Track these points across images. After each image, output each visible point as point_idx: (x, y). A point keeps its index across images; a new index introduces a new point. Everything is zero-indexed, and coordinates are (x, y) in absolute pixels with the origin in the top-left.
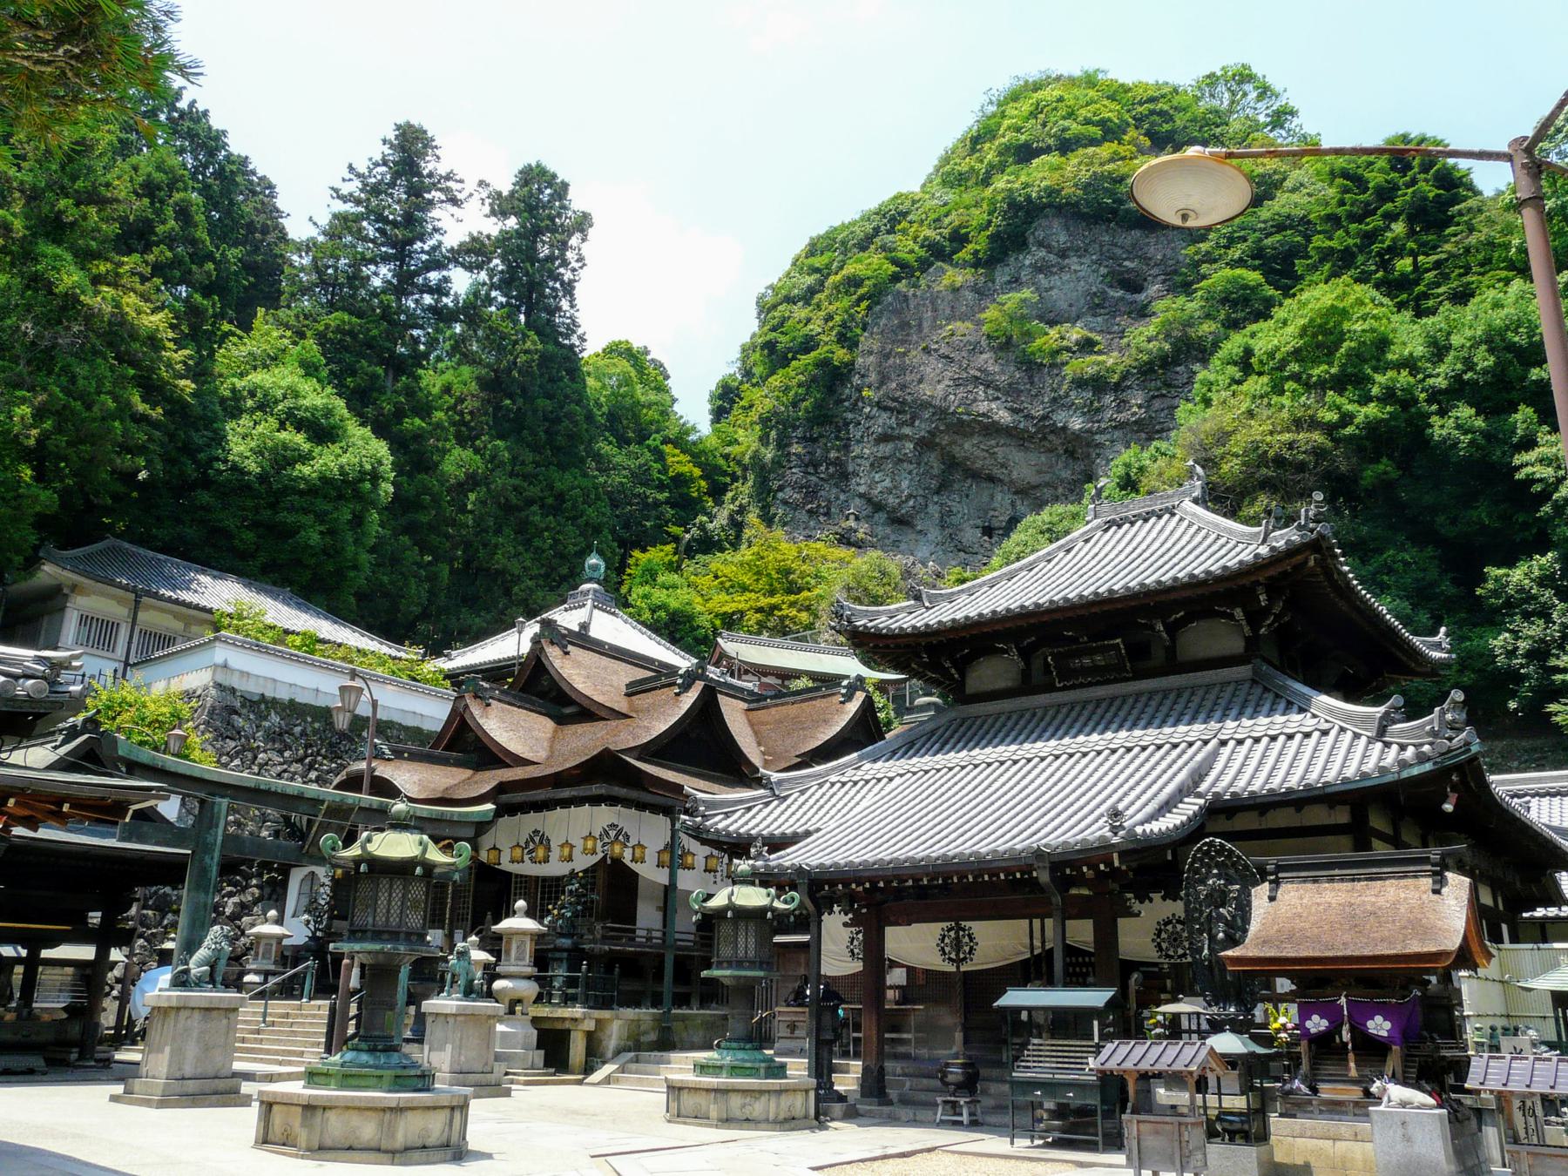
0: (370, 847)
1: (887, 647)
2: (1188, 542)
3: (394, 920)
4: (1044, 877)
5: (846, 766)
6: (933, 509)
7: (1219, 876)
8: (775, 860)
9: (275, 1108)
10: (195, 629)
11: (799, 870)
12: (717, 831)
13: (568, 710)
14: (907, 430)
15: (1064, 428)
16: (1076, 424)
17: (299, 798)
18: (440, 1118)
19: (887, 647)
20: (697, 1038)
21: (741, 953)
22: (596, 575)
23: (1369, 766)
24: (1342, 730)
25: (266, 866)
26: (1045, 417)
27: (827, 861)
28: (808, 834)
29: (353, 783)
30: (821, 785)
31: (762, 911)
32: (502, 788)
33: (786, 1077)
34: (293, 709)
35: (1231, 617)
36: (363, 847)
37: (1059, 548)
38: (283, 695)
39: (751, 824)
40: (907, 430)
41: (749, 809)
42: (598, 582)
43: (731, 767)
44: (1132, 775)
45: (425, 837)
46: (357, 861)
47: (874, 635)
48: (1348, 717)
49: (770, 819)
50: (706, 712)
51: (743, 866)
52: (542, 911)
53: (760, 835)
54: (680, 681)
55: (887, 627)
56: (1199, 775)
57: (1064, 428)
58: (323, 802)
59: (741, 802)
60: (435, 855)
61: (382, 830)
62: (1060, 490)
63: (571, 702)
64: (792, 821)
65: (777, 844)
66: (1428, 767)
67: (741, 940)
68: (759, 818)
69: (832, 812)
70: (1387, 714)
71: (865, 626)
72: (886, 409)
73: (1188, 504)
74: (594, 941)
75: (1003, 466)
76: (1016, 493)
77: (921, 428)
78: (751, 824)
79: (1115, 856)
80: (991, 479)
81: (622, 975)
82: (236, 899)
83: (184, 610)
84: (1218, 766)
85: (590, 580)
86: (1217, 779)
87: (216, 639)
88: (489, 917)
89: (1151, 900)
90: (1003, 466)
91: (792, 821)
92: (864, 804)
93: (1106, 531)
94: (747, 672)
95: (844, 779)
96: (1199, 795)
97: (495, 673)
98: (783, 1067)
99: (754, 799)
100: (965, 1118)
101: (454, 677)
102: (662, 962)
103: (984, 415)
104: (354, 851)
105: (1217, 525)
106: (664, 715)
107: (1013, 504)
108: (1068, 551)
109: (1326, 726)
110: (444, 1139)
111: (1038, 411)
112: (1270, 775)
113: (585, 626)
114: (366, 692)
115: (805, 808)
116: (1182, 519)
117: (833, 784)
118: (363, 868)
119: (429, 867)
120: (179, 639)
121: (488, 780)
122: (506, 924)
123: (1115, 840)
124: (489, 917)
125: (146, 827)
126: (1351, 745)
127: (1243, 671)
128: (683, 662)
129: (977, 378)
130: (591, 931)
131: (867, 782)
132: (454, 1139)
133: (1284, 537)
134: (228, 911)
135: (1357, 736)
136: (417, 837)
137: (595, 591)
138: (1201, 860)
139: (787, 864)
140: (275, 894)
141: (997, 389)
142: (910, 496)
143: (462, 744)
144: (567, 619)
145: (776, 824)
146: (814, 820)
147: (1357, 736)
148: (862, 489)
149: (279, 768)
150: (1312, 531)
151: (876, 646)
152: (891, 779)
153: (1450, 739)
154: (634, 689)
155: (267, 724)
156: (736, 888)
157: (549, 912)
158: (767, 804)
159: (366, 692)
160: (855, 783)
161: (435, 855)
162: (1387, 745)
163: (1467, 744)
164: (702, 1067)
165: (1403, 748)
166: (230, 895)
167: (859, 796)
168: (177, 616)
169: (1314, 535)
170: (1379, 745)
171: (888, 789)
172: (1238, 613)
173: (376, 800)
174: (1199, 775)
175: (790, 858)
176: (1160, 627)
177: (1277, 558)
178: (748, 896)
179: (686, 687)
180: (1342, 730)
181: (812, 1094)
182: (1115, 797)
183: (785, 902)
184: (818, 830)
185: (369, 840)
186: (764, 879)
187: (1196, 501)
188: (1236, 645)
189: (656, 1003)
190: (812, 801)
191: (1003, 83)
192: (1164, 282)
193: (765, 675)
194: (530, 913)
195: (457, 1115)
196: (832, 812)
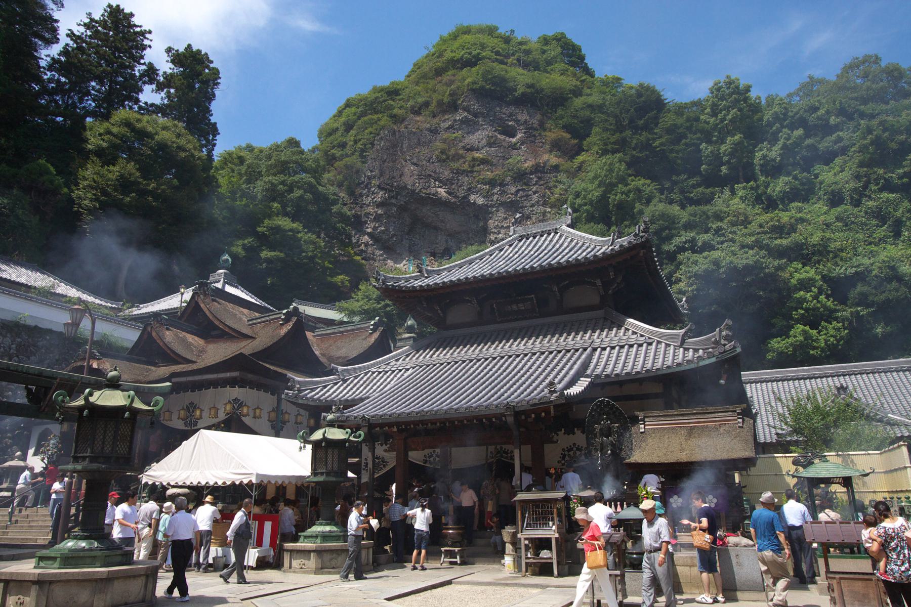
0: (91, 399)
2: (574, 242)
4: (510, 420)
5: (380, 362)
6: (406, 243)
7: (607, 419)
8: (347, 413)
9: (11, 584)
12: (307, 399)
14: (394, 201)
15: (474, 203)
16: (481, 201)
18: (140, 582)
20: (450, 543)
21: (330, 467)
23: (679, 359)
24: (658, 342)
26: (465, 197)
29: (80, 369)
30: (366, 374)
31: (343, 441)
35: (594, 285)
36: (86, 399)
37: (496, 249)
40: (394, 201)
41: (325, 387)
44: (547, 366)
46: (80, 409)
48: (663, 335)
54: (283, 317)
56: (585, 365)
57: (474, 203)
58: (56, 379)
60: (139, 405)
62: (471, 235)
64: (350, 393)
65: (349, 404)
66: (714, 360)
68: (331, 391)
69: (375, 387)
70: (686, 333)
72: (383, 189)
73: (564, 227)
75: (442, 221)
76: (449, 235)
77: (402, 200)
79: (552, 407)
80: (436, 228)
84: (594, 361)
86: (595, 368)
89: (574, 433)
90: (442, 221)
91: (350, 393)
93: (520, 241)
96: (587, 376)
99: (328, 381)
100: (458, 560)
103: (434, 195)
104: (80, 402)
105: (583, 237)
107: (447, 241)
108: (501, 250)
109: (651, 341)
110: (141, 597)
111: (461, 194)
112: (624, 366)
115: (358, 386)
116: (561, 236)
117: (373, 373)
119: (135, 412)
121: (164, 370)
123: (552, 398)
126: (665, 350)
127: (600, 313)
129: (430, 176)
131: (394, 371)
132: (148, 597)
133: (624, 241)
135: (667, 345)
138: (595, 410)
141: (440, 181)
142: (394, 235)
147: (667, 345)
148: (369, 230)
150: (642, 237)
152: (407, 370)
153: (725, 345)
154: (252, 324)
160: (387, 372)
162: (686, 349)
163: (734, 347)
165: (696, 350)
169: (644, 239)
170: (681, 349)
171: (406, 375)
172: (598, 282)
174: (585, 365)
175: (358, 411)
176: (556, 289)
177: (623, 250)
178: (334, 433)
180: (658, 342)
181: (371, 550)
182: (552, 376)
184: (368, 398)
185: (91, 394)
187: (568, 226)
188: (596, 300)
190: (361, 382)
191: (447, 30)
192: (525, 133)
195: (151, 580)
196: (375, 387)
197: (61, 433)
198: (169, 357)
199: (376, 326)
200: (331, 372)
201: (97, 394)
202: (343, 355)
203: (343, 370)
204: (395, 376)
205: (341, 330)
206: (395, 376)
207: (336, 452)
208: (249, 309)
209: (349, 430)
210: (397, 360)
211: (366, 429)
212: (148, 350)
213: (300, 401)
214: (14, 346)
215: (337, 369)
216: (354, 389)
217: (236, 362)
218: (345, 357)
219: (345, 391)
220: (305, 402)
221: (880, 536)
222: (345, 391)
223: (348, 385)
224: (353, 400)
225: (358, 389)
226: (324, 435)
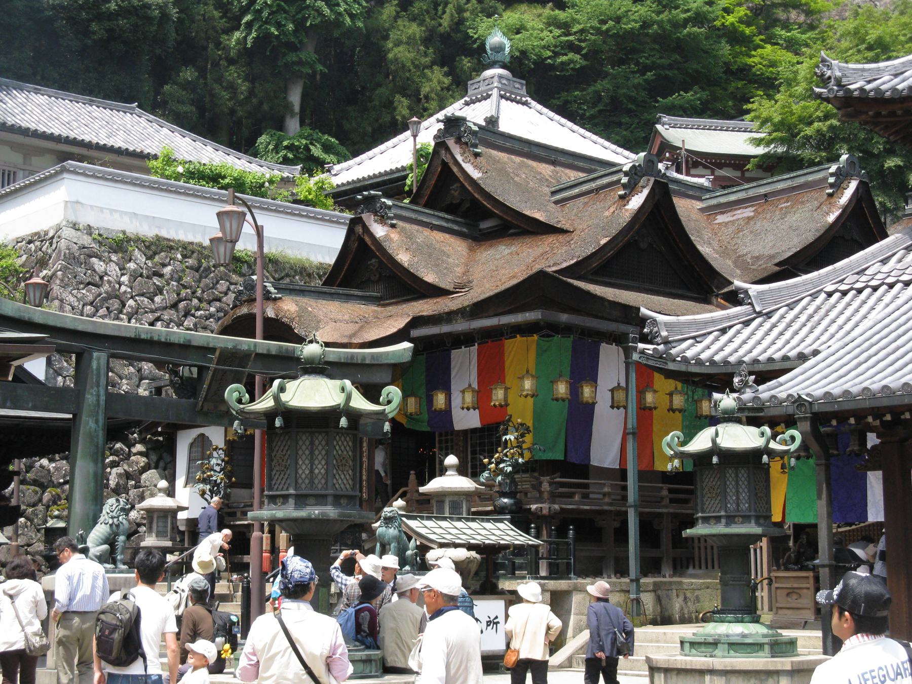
0: (284, 397)
1: (893, 114)
3: (319, 482)
8: (765, 391)
10: (35, 161)
11: (799, 401)
12: (685, 360)
13: (485, 225)
17: (186, 348)
19: (893, 114)
22: (499, 57)
25: (151, 428)
27: (836, 389)
28: (802, 358)
32: (417, 321)
33: (798, 655)
34: (156, 247)
36: (276, 398)
38: (148, 231)
39: (728, 350)
41: (724, 331)
42: (504, 66)
43: (700, 282)
45: (348, 383)
46: (270, 415)
47: (875, 100)
49: (751, 342)
50: (660, 214)
51: (727, 401)
52: (474, 467)
53: (740, 362)
54: (625, 180)
55: (894, 89)
58: (213, 350)
59: (713, 322)
60: (359, 402)
61: (294, 378)
63: (488, 215)
64: (780, 343)
65: (766, 373)
67: (731, 490)
69: (832, 329)
71: (861, 89)
74: (539, 500)
78: (728, 350)
81: (577, 539)
82: (119, 470)
83: (20, 139)
85: (491, 65)
87: (64, 170)
88: (412, 476)
91: (780, 343)
92: (874, 316)
94: (696, 165)
95: (844, 287)
97: (391, 184)
98: (792, 643)
101: (347, 197)
102: (625, 523)
104: (265, 403)
106: (598, 222)
113: (492, 121)
114: (249, 217)
115: (796, 326)
117: (830, 295)
118: (278, 423)
119: (355, 416)
120: (20, 174)
121: (396, 318)
122: (436, 484)
124: (412, 476)
125: (20, 389)
128: (625, 159)
130: (537, 487)
134: (112, 483)
136: (338, 383)
137: (501, 77)
139: (783, 395)
140: (163, 458)
143: (362, 271)
144: (475, 114)
145: (760, 348)
146: (809, 340)
149: (151, 317)
151: (878, 114)
154: (562, 196)
155: (132, 265)
156: (721, 427)
157: (484, 468)
158: (747, 323)
159: (249, 217)
161: (359, 402)
164: (693, 644)
166: (114, 465)
167: (866, 308)
168: (14, 146)
173: (274, 345)
175: (784, 388)
179: (632, 188)
183: (784, 442)
184: (816, 353)
185: (282, 389)
186: (752, 416)
189: (622, 571)
190: (803, 318)
193: (720, 166)
194: (462, 470)
196: (832, 329)
197: (227, 442)
198: (402, 285)
199: (842, 177)
200: (735, 298)
201: (291, 385)
202: (768, 251)
203: (760, 293)
204: (880, 300)
205: (762, 190)
206: (880, 300)
207: (743, 473)
208: (554, 163)
209: (767, 430)
210: (884, 262)
211: (806, 426)
212: (362, 271)
213: (671, 366)
214: (125, 279)
215: (746, 292)
216: (788, 334)
217: (537, 289)
218: (772, 257)
219: (769, 339)
220: (683, 368)
221: (514, 598)
222: (769, 339)
223: (774, 326)
224: (785, 358)
225: (796, 333)
226: (714, 441)
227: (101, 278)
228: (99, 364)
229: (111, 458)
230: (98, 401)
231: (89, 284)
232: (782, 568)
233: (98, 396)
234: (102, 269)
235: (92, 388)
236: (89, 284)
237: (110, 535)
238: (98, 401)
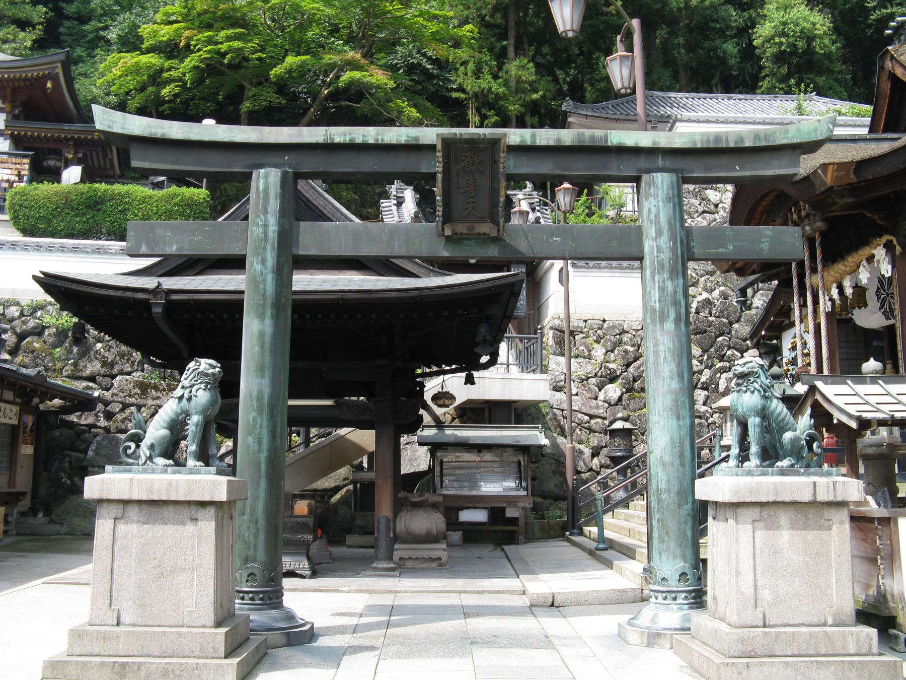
28: (764, 616)
227: (716, 206)
228: (266, 183)
229: (721, 364)
230: (265, 233)
231: (704, 212)
232: (683, 77)
233: (266, 226)
234: (717, 198)
235: (258, 216)
236: (704, 212)
237: (178, 415)
238: (265, 233)
